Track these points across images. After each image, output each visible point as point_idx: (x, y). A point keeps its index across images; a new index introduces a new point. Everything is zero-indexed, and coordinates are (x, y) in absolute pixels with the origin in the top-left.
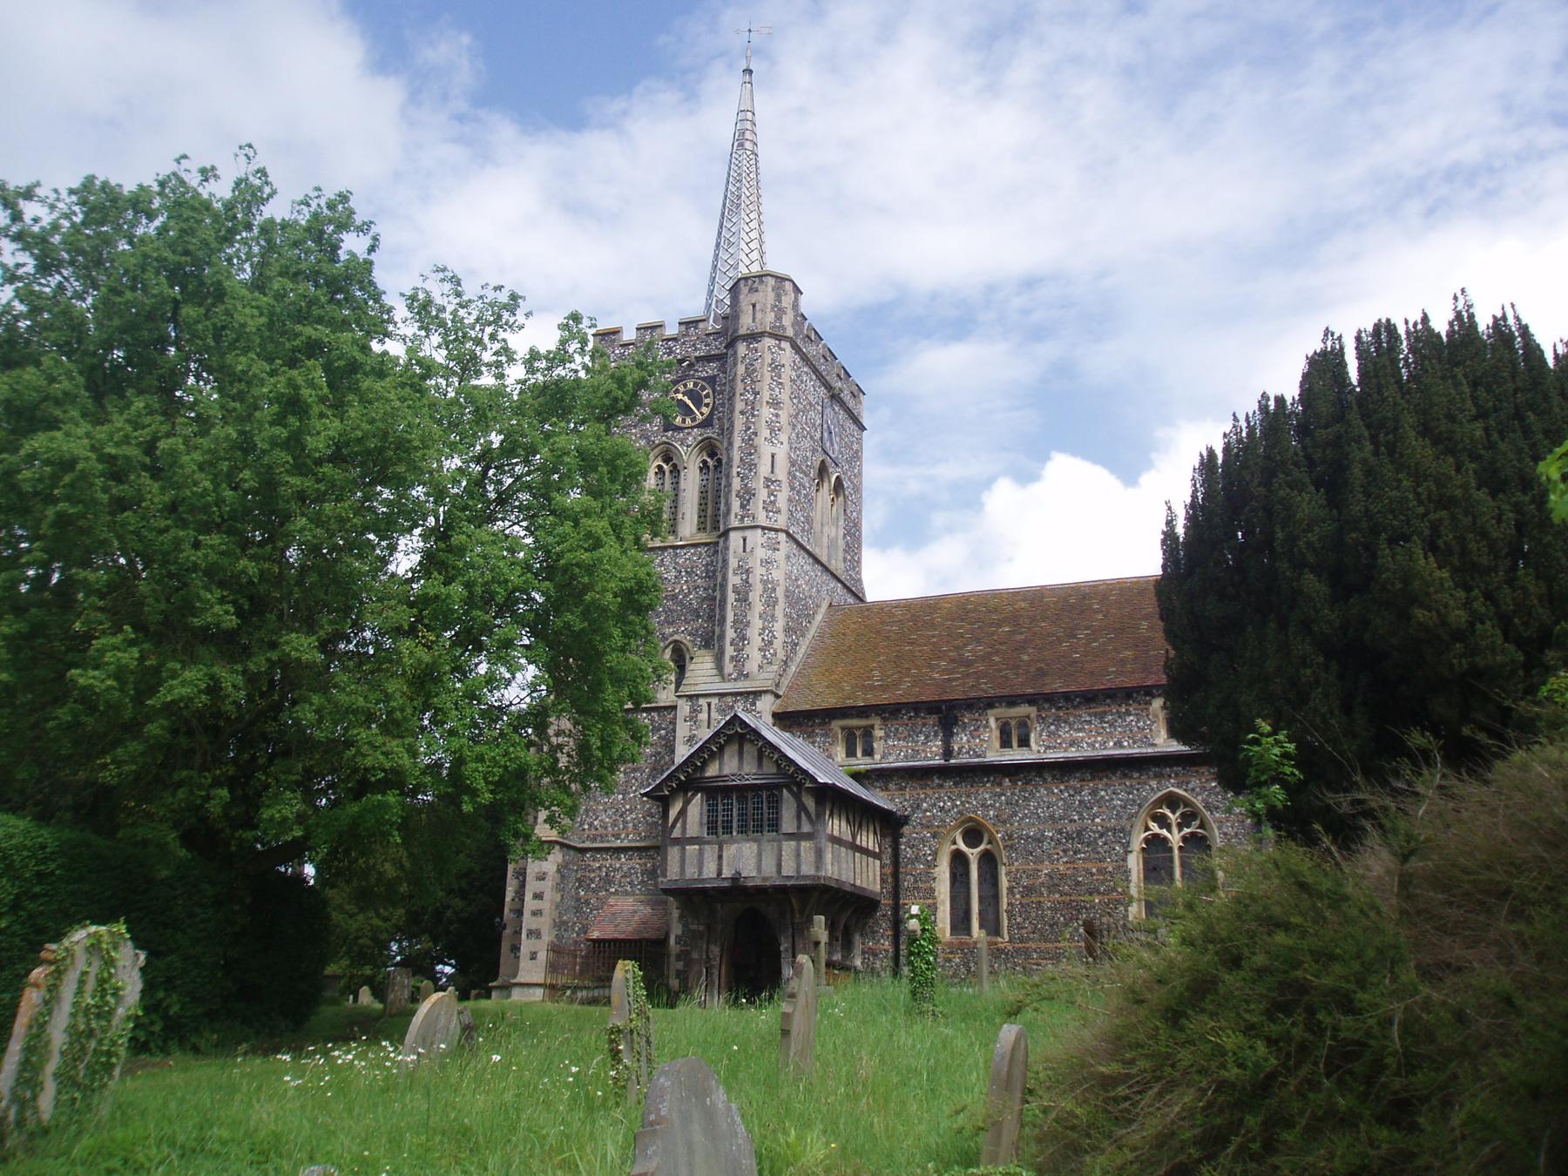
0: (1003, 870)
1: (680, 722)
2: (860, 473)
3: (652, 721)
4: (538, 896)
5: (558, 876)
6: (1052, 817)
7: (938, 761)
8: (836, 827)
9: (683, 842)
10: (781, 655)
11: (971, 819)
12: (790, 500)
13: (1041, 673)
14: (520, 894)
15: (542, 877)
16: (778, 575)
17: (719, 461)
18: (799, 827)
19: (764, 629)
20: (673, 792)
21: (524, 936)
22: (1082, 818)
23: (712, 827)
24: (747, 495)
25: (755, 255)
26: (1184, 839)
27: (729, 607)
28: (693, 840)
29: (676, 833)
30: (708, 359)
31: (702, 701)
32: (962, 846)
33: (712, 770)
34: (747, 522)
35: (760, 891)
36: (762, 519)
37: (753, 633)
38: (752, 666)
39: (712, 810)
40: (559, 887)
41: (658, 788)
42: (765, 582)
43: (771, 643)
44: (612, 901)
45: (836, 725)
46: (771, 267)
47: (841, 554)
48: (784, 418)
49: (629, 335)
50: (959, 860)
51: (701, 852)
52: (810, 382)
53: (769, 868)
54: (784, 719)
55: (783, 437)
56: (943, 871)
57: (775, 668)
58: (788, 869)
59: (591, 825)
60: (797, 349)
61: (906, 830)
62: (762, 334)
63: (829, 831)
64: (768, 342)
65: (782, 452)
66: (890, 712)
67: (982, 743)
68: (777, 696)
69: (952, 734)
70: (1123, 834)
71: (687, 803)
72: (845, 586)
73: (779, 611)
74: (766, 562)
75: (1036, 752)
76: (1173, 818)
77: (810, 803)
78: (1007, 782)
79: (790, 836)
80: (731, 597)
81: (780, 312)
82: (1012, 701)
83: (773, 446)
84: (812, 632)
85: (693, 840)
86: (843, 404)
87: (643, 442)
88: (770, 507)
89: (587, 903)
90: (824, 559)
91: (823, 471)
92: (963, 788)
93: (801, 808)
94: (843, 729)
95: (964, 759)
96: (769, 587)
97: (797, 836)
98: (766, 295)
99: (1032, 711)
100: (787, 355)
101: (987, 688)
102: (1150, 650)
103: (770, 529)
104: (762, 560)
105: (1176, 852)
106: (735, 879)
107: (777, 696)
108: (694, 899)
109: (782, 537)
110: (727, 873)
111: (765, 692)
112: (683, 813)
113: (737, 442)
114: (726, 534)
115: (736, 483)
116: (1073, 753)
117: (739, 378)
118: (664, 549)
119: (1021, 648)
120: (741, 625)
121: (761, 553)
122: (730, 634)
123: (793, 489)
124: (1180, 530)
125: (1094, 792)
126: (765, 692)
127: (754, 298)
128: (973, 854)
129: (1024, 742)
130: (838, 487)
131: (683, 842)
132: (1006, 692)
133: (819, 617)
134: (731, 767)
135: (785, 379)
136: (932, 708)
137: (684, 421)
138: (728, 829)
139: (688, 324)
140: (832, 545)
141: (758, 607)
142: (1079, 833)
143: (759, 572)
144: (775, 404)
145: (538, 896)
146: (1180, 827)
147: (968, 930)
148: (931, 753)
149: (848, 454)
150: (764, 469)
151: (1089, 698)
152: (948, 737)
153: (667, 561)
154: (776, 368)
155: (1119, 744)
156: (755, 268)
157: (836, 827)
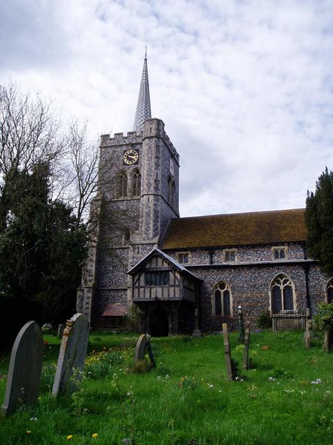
0: (231, 296)
7: (208, 264)
15: (88, 298)
16: (159, 209)
17: (140, 175)
29: (137, 285)
30: (137, 144)
33: (148, 266)
45: (177, 253)
48: (160, 162)
49: (112, 136)
51: (145, 290)
53: (166, 296)
60: (163, 140)
67: (220, 259)
73: (159, 219)
75: (237, 261)
77: (178, 276)
78: (233, 270)
79: (172, 286)
82: (230, 247)
85: (142, 287)
92: (220, 272)
95: (216, 264)
99: (236, 250)
102: (302, 232)
109: (160, 197)
110: (153, 296)
112: (139, 279)
118: (123, 201)
129: (233, 260)
130: (174, 184)
131: (139, 287)
135: (160, 150)
139: (129, 133)
145: (87, 303)
148: (206, 262)
151: (253, 246)
155: (261, 260)
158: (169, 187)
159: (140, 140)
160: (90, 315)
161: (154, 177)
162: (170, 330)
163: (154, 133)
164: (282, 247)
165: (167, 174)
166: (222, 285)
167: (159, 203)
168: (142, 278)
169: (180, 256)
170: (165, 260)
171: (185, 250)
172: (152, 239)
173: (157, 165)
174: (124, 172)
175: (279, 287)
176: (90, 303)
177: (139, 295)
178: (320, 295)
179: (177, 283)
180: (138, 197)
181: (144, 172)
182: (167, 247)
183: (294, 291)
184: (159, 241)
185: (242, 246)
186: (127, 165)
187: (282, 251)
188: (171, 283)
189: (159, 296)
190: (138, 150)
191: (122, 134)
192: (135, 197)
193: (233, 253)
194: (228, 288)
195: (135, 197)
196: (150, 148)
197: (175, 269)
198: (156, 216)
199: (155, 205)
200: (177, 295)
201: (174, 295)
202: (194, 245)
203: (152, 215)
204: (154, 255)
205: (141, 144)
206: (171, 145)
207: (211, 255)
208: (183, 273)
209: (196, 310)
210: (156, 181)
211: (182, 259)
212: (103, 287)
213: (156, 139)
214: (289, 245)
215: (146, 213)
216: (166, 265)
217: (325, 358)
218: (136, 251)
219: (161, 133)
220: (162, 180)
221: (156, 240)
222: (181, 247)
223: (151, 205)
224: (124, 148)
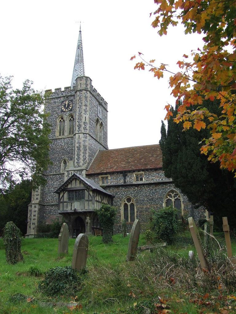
0: (135, 207)
1: (65, 177)
2: (107, 121)
3: (59, 177)
4: (34, 216)
5: (39, 211)
6: (146, 195)
8: (97, 198)
9: (63, 202)
10: (88, 161)
11: (129, 196)
12: (89, 127)
13: (146, 164)
14: (31, 215)
15: (35, 211)
16: (87, 144)
17: (74, 119)
19: (84, 156)
20: (61, 191)
21: (32, 224)
22: (153, 196)
23: (69, 199)
24: (79, 126)
25: (82, 73)
26: (175, 200)
27: (76, 151)
28: (65, 202)
29: (62, 201)
30: (71, 96)
31: (70, 172)
32: (127, 202)
33: (69, 186)
34: (80, 132)
35: (80, 213)
36: (83, 132)
37: (81, 157)
38: (81, 164)
39: (69, 195)
40: (39, 214)
41: (57, 190)
42: (84, 145)
43: (85, 159)
44: (51, 216)
45: (100, 177)
46: (86, 75)
47: (102, 139)
48: (88, 109)
50: (126, 205)
51: (67, 204)
52: (94, 101)
54: (88, 176)
55: (88, 113)
56: (122, 208)
57: (86, 164)
59: (46, 200)
60: (90, 93)
61: (114, 199)
62: (83, 90)
63: (96, 199)
64: (84, 92)
65: (87, 116)
66: (112, 173)
67: (132, 179)
68: (87, 171)
69: (126, 178)
70: (161, 199)
71: (64, 194)
72: (103, 146)
74: (84, 141)
75: (144, 181)
76: (173, 195)
77: (91, 193)
78: (136, 188)
80: (76, 149)
81: (87, 85)
82: (139, 171)
83: (85, 117)
84: (95, 157)
86: (102, 106)
87: (56, 115)
88: (85, 129)
89: (46, 217)
90: (98, 140)
91: (97, 121)
93: (89, 194)
94: (101, 177)
95: (128, 183)
96: (85, 147)
97: (88, 201)
98: (83, 81)
99: (143, 173)
100: (89, 95)
101: (134, 168)
102: (158, 160)
103: (85, 134)
104: (82, 140)
105: (173, 202)
106: (75, 210)
107: (87, 171)
108: (66, 215)
109: (88, 135)
111: (84, 169)
112: (63, 196)
113: (77, 114)
114: (75, 135)
115: (77, 123)
116: (152, 182)
117: (78, 100)
119: (141, 159)
120: (78, 155)
121: (83, 139)
122: (76, 157)
123: (90, 125)
124: (167, 128)
125: (156, 190)
126: (84, 169)
127: (81, 82)
128: (129, 204)
129: (141, 179)
130: (101, 124)
131: (63, 202)
132: (138, 168)
133: (97, 153)
134: (75, 185)
135: (88, 100)
136: (121, 172)
137: (66, 110)
138: (73, 199)
139: (66, 88)
140: (100, 137)
141: (82, 151)
142: (152, 199)
143: (82, 143)
144: (86, 105)
145: (34, 216)
146: (174, 197)
147: (128, 220)
148: (121, 182)
149: (104, 117)
150: (83, 120)
152: (125, 178)
153: (62, 141)
154: (86, 97)
156: (82, 75)
157: (97, 198)
159: (73, 93)
167: (87, 139)
168: (66, 195)
171: (106, 174)
176: (37, 215)
177: (63, 208)
179: (90, 199)
180: (72, 136)
185: (147, 170)
186: (64, 112)
188: (86, 198)
191: (60, 89)
193: (107, 177)
194: (133, 201)
207: (125, 176)
215: (77, 147)
216: (82, 186)
219: (89, 87)
220: (90, 122)
224: (62, 99)
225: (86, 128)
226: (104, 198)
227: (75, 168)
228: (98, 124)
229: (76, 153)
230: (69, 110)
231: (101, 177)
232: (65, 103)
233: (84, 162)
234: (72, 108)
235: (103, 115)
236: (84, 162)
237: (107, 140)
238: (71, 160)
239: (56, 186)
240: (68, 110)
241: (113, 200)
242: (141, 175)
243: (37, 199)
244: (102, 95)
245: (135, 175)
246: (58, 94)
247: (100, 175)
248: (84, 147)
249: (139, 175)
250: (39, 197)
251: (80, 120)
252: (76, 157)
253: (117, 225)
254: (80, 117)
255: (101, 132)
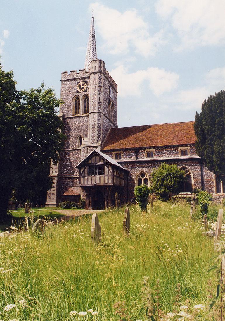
8: (116, 174)
12: (103, 107)
16: (101, 122)
18: (108, 174)
19: (98, 133)
21: (51, 195)
29: (83, 175)
33: (90, 162)
42: (98, 124)
43: (100, 136)
45: (114, 153)
48: (102, 89)
51: (88, 179)
52: (107, 83)
55: (102, 93)
58: (106, 182)
59: (64, 173)
82: (150, 148)
85: (86, 176)
89: (64, 188)
93: (109, 170)
94: (115, 153)
99: (154, 150)
108: (85, 188)
110: (94, 183)
112: (84, 171)
123: (104, 104)
128: (143, 179)
131: (84, 177)
133: (109, 131)
137: (81, 91)
148: (134, 159)
149: (114, 98)
157: (116, 174)
158: (110, 105)
159: (88, 75)
160: (55, 195)
161: (97, 100)
162: (105, 205)
163: (97, 70)
164: (186, 148)
165: (108, 98)
166: (143, 174)
169: (116, 154)
170: (102, 158)
172: (97, 143)
173: (100, 92)
174: (77, 97)
175: (190, 175)
178: (210, 181)
180: (87, 114)
181: (91, 97)
182: (106, 148)
183: (192, 178)
184: (101, 144)
187: (186, 150)
188: (106, 174)
189: (98, 182)
190: (86, 82)
192: (85, 115)
195: (85, 115)
196: (95, 80)
197: (107, 163)
198: (99, 127)
199: (98, 120)
200: (110, 182)
201: (108, 182)
202: (125, 147)
203: (96, 127)
204: (95, 154)
205: (88, 78)
206: (111, 78)
208: (114, 167)
209: (116, 193)
210: (99, 103)
211: (117, 157)
212: (64, 176)
213: (99, 74)
214: (190, 146)
217: (104, 216)
218: (86, 151)
220: (104, 102)
221: (99, 143)
222: (116, 148)
223: (96, 120)
225: (100, 107)
226: (121, 173)
227: (91, 145)
228: (110, 104)
229: (91, 131)
230: (84, 90)
231: (115, 153)
232: (80, 84)
233: (99, 139)
234: (87, 89)
235: (114, 96)
236: (99, 139)
237: (117, 119)
238: (86, 136)
239: (73, 161)
240: (83, 90)
241: (128, 175)
242: (152, 152)
243: (56, 172)
244: (114, 78)
245: (147, 151)
246: (73, 76)
247: (113, 151)
248: (99, 125)
249: (150, 152)
250: (57, 170)
251: (95, 100)
252: (91, 134)
253: (132, 197)
254: (95, 97)
255: (112, 111)
